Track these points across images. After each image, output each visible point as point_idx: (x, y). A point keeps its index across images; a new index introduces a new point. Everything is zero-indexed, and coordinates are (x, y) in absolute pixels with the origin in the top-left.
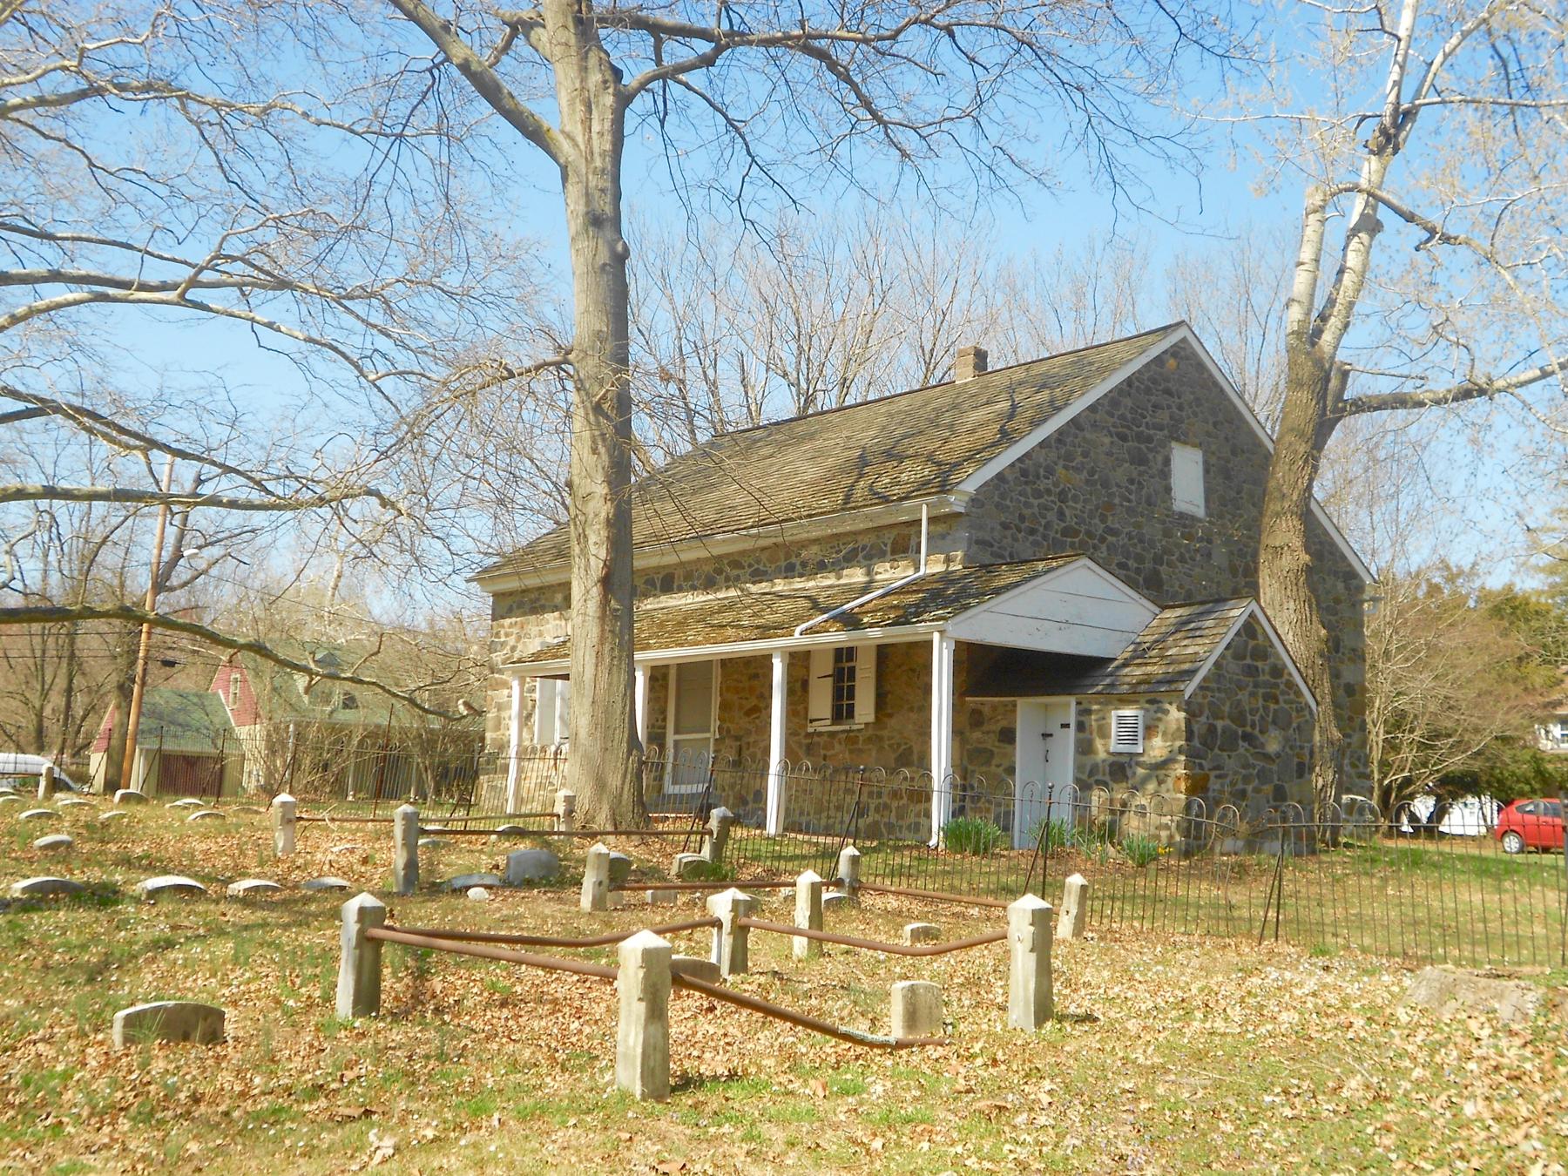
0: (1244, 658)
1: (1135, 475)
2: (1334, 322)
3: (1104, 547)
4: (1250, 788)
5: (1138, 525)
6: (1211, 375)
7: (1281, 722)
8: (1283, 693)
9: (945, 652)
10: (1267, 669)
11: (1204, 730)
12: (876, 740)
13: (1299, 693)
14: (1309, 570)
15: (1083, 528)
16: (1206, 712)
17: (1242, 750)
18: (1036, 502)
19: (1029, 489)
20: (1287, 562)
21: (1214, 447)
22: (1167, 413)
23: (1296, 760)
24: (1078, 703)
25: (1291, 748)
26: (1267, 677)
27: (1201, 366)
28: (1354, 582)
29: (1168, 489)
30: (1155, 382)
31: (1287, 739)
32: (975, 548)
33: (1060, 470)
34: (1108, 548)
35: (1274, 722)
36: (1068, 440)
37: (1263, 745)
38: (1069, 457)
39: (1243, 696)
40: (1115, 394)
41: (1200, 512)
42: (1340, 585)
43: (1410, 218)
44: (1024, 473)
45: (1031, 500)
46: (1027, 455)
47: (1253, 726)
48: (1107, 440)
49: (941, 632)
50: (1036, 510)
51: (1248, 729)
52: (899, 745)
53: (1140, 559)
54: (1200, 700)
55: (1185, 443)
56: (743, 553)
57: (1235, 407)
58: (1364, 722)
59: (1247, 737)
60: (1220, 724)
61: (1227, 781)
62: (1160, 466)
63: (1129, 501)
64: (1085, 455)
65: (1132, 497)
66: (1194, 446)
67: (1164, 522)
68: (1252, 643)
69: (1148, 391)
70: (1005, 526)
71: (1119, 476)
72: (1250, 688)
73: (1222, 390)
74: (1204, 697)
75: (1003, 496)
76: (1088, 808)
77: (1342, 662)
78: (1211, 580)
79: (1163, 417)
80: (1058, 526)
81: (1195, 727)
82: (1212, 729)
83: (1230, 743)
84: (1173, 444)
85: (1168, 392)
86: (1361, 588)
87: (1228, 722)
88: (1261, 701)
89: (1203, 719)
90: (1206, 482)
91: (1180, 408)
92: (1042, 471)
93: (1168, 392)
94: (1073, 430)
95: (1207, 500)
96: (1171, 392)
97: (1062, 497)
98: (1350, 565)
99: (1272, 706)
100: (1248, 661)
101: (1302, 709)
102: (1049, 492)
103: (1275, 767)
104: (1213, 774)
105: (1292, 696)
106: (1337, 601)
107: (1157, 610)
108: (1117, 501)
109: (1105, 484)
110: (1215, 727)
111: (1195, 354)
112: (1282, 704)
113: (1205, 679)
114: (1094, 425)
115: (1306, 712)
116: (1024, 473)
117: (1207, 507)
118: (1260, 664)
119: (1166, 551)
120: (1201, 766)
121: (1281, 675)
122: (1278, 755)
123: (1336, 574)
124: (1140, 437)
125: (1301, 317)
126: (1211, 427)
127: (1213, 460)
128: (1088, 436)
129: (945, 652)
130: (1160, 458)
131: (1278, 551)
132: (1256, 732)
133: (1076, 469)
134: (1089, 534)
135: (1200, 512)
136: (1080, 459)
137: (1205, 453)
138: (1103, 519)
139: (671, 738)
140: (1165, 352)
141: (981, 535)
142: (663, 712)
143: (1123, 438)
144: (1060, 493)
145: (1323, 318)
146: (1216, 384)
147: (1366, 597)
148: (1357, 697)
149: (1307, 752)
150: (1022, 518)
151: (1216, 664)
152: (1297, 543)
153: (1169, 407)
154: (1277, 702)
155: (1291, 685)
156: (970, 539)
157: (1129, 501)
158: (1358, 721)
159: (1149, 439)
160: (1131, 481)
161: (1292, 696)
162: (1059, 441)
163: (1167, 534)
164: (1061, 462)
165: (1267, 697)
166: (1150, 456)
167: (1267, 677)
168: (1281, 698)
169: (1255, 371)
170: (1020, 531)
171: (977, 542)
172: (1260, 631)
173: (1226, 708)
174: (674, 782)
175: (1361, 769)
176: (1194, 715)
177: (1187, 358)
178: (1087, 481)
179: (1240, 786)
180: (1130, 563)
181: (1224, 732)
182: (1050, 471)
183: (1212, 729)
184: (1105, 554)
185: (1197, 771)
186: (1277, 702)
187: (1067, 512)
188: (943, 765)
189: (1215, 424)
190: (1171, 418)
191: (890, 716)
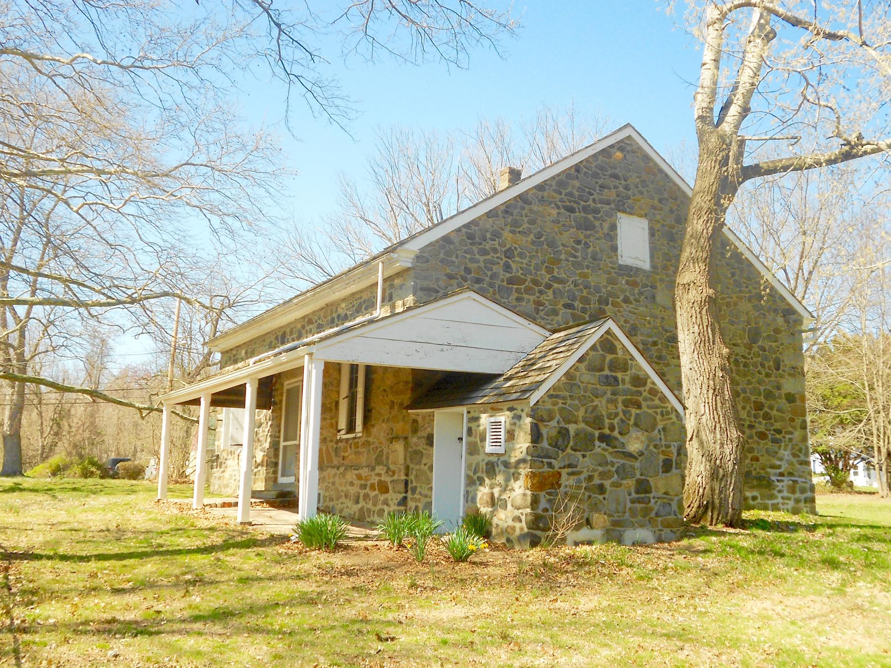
0: (602, 370)
1: (581, 237)
2: (734, 110)
3: (550, 292)
4: (607, 483)
5: (584, 276)
6: (656, 164)
7: (645, 425)
8: (645, 400)
9: (314, 371)
10: (627, 379)
11: (554, 433)
12: (367, 444)
13: (664, 399)
14: (711, 301)
15: (529, 278)
16: (558, 417)
17: (597, 450)
18: (482, 258)
19: (475, 249)
20: (694, 295)
21: (658, 217)
22: (614, 191)
23: (662, 457)
24: (469, 412)
25: (655, 446)
26: (628, 386)
27: (647, 158)
28: (794, 317)
29: (615, 249)
30: (602, 168)
31: (650, 440)
32: (419, 293)
33: (506, 234)
34: (554, 293)
35: (636, 425)
36: (515, 212)
37: (623, 445)
38: (516, 224)
39: (602, 405)
40: (563, 177)
41: (647, 266)
42: (780, 320)
43: (796, 22)
44: (471, 237)
45: (477, 256)
46: (474, 222)
47: (612, 428)
48: (554, 212)
49: (311, 354)
50: (482, 264)
51: (606, 431)
52: (377, 448)
53: (585, 301)
54: (549, 406)
55: (631, 214)
56: (314, 313)
57: (679, 188)
58: (805, 421)
59: (603, 438)
60: (572, 428)
61: (582, 477)
62: (606, 230)
63: (575, 257)
64: (532, 222)
65: (579, 254)
66: (640, 216)
67: (609, 273)
68: (609, 357)
69: (595, 175)
70: (450, 277)
71: (566, 238)
72: (609, 395)
73: (667, 175)
74: (554, 404)
75: (448, 254)
76: (474, 499)
77: (782, 376)
78: (656, 317)
79: (611, 195)
80: (504, 275)
81: (544, 431)
82: (563, 433)
83: (585, 443)
84: (619, 215)
85: (615, 176)
86: (799, 321)
87: (582, 425)
88: (620, 407)
89: (553, 423)
90: (651, 243)
91: (627, 188)
92: (488, 235)
93: (615, 176)
94: (520, 203)
95: (652, 256)
96: (616, 176)
97: (509, 254)
98: (789, 304)
99: (634, 411)
100: (606, 372)
101: (668, 413)
102: (495, 251)
103: (637, 464)
104: (564, 472)
105: (657, 402)
106: (777, 331)
107: (547, 334)
108: (563, 257)
109: (552, 244)
110: (567, 430)
111: (640, 148)
112: (645, 409)
113: (554, 388)
114: (542, 200)
115: (673, 416)
116: (471, 237)
117: (652, 262)
118: (619, 375)
119: (610, 294)
120: (550, 465)
121: (645, 384)
122: (641, 454)
123: (775, 311)
124: (585, 209)
125: (705, 105)
126: (656, 202)
127: (658, 226)
128: (535, 208)
129: (314, 371)
130: (606, 226)
131: (687, 287)
132: (616, 433)
133: (525, 233)
134: (536, 283)
135: (647, 266)
136: (526, 225)
137: (650, 221)
138: (550, 270)
139: (282, 444)
140: (612, 146)
141: (425, 284)
142: (279, 426)
143: (571, 210)
144: (506, 252)
145: (725, 108)
146: (661, 171)
147: (803, 328)
148: (798, 403)
149: (674, 450)
150: (468, 270)
151: (567, 374)
152: (702, 280)
153: (615, 187)
154: (639, 407)
155: (654, 392)
156: (415, 287)
157: (575, 257)
158: (798, 421)
159: (596, 211)
160: (578, 242)
161: (657, 402)
162: (506, 212)
163: (612, 282)
164: (508, 228)
165: (626, 403)
166: (597, 223)
167: (628, 386)
168: (644, 404)
169: (682, 157)
170: (465, 280)
171: (422, 289)
172: (619, 346)
173: (581, 413)
174: (283, 475)
175: (802, 458)
176: (542, 420)
177: (633, 152)
178: (533, 243)
179: (597, 481)
180: (576, 304)
181: (577, 435)
182: (496, 235)
183: (563, 433)
184: (551, 297)
185: (546, 469)
186: (639, 407)
187: (513, 265)
188: (309, 468)
189: (660, 201)
190: (618, 196)
191: (373, 426)
